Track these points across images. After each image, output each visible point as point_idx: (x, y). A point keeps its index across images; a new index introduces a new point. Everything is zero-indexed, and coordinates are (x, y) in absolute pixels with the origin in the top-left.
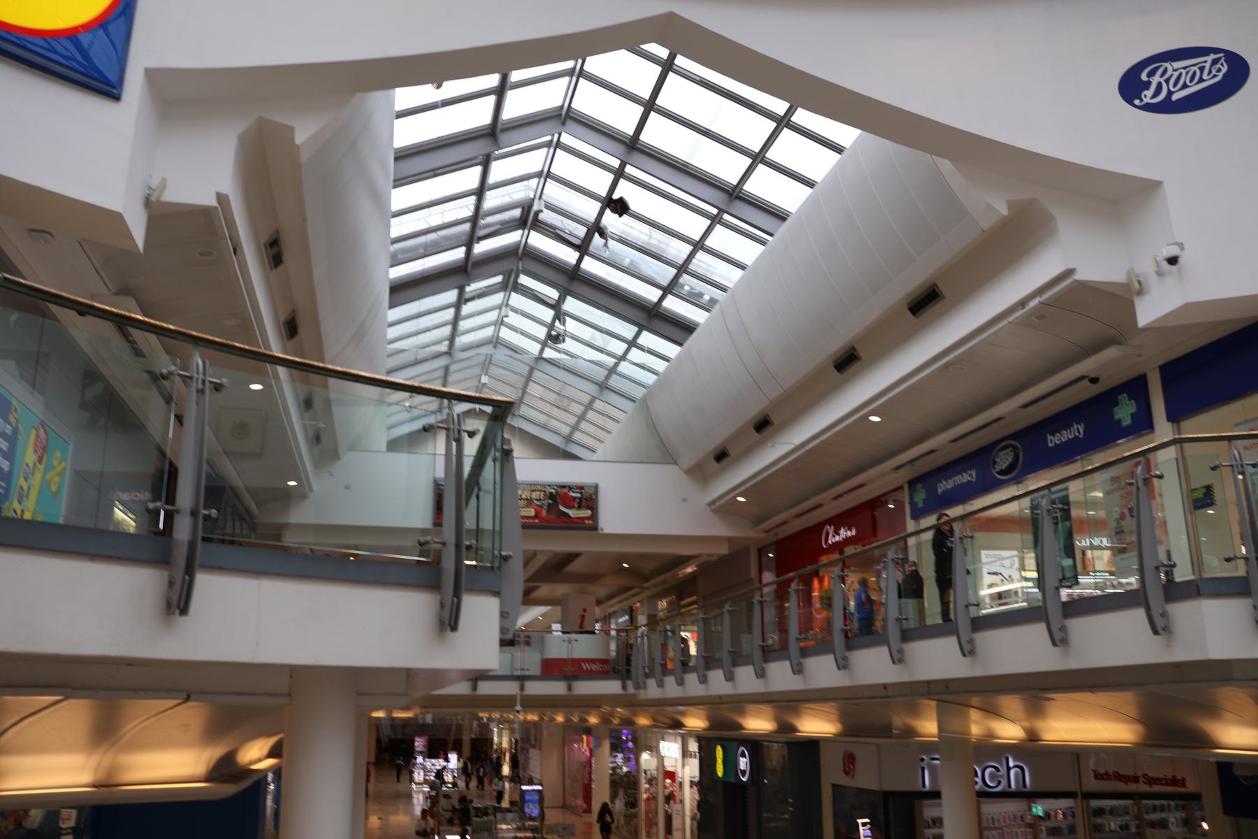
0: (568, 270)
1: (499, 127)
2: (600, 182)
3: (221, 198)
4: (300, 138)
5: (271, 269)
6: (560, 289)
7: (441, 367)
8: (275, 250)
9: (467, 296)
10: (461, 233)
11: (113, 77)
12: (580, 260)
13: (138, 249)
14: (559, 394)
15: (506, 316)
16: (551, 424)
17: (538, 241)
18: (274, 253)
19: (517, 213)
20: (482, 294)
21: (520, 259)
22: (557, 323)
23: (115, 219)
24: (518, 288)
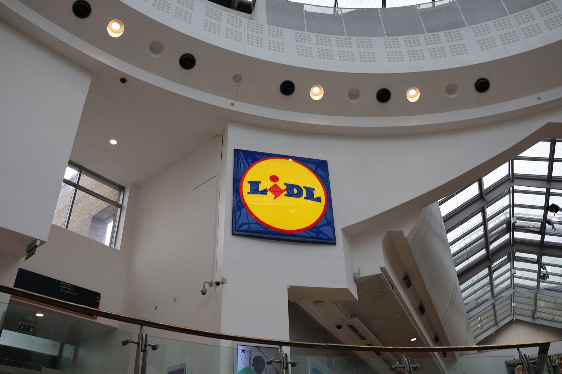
0: (539, 244)
1: (484, 193)
2: (540, 200)
3: (382, 269)
4: (406, 234)
5: (408, 289)
6: (537, 254)
7: (491, 305)
8: (407, 280)
9: (493, 269)
10: (481, 243)
11: (332, 237)
12: (543, 238)
13: (356, 300)
14: (555, 303)
15: (516, 273)
16: (555, 318)
17: (518, 235)
18: (407, 281)
19: (504, 226)
20: (500, 267)
21: (513, 246)
22: (542, 270)
23: (346, 291)
24: (516, 259)
